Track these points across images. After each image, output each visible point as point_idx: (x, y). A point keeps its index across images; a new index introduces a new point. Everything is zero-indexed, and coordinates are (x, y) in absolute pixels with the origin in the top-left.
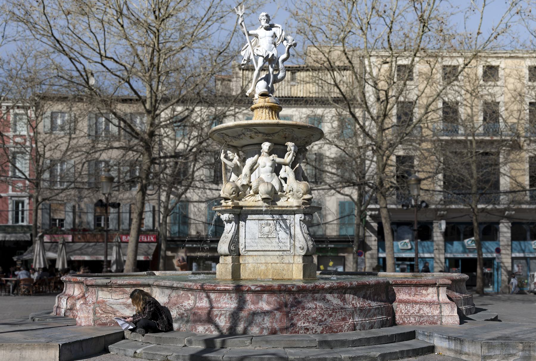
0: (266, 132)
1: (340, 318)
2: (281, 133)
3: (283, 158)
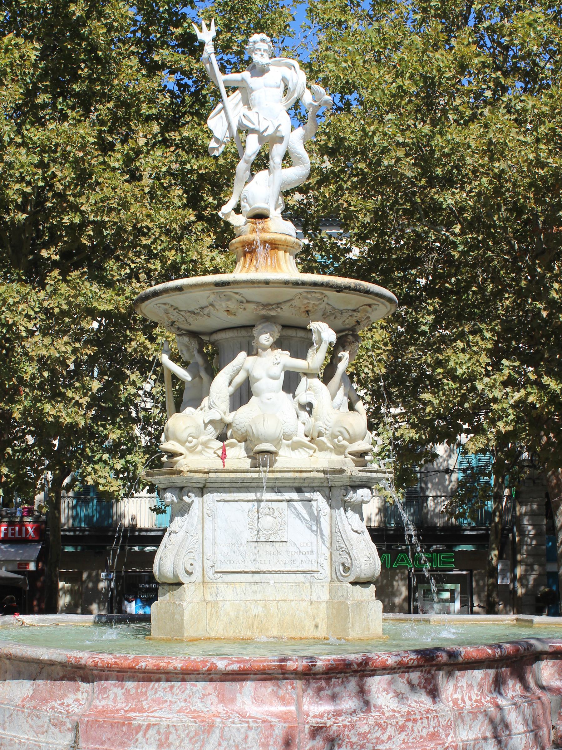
0: (263, 300)
1: (424, 733)
2: (297, 302)
3: (304, 357)
